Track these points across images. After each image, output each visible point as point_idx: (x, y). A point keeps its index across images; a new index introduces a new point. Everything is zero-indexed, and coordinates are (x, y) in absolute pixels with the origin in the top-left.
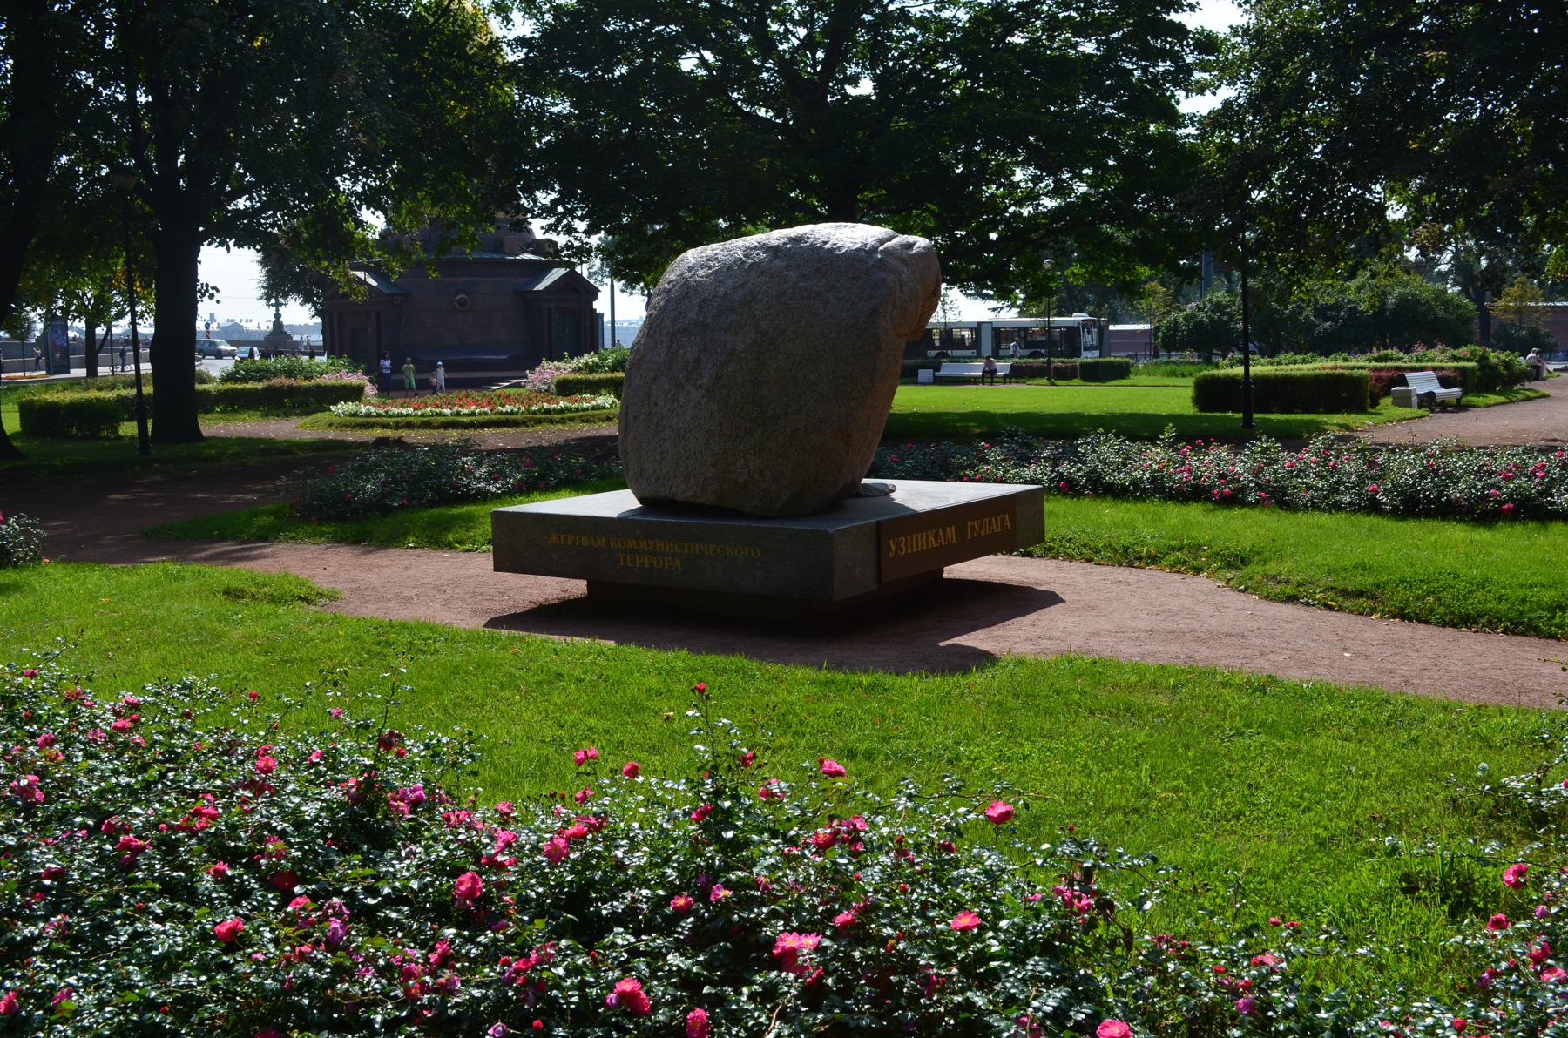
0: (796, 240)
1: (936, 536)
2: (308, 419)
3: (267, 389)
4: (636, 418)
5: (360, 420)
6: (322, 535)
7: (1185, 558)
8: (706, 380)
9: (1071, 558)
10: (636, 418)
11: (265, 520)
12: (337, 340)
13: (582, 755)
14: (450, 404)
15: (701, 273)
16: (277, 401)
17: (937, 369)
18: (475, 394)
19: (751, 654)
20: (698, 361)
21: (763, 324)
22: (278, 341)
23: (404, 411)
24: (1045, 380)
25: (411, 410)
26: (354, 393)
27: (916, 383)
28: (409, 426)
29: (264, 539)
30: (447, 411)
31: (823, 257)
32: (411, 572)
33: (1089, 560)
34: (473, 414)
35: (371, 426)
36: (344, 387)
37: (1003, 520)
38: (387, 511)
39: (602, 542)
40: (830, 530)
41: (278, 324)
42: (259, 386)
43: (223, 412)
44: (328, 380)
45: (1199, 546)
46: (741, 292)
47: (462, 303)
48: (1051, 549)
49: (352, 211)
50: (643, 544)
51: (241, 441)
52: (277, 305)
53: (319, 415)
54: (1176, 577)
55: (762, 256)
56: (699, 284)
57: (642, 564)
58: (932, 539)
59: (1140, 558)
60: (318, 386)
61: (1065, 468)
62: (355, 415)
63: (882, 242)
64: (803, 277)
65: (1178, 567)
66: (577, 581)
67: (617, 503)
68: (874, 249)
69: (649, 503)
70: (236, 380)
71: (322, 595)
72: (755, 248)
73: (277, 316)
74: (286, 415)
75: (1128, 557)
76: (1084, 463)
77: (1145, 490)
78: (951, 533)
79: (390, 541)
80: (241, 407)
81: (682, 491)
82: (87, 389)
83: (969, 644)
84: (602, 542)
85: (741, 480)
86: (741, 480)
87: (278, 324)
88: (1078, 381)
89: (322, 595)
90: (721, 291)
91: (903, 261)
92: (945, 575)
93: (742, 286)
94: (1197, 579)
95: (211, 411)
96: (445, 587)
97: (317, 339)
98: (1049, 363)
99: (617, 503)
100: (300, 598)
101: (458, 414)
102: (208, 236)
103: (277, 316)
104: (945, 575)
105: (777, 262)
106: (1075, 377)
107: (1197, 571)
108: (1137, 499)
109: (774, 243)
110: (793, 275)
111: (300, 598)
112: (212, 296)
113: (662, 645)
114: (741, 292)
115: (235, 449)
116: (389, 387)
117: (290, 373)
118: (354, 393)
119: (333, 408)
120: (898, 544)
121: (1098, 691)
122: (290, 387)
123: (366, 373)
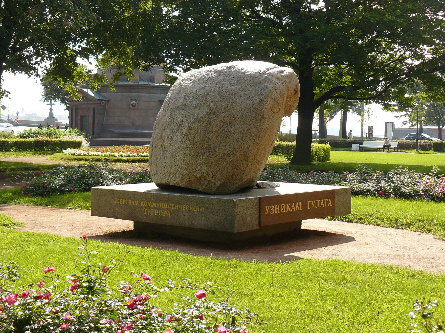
0: (229, 68)
1: (291, 207)
2: (52, 156)
3: (36, 142)
4: (156, 147)
5: (75, 157)
6: (32, 202)
7: (423, 226)
8: (185, 130)
9: (370, 224)
10: (156, 147)
11: (8, 195)
12: (76, 122)
13: (47, 269)
14: (119, 151)
15: (187, 82)
16: (39, 147)
17: (361, 144)
18: (131, 147)
19: (180, 251)
20: (182, 121)
21: (211, 105)
22: (51, 121)
23: (97, 154)
24: (415, 151)
25: (99, 153)
26: (77, 145)
27: (351, 150)
28: (98, 160)
29: (5, 203)
30: (116, 154)
31: (241, 77)
32: (63, 218)
33: (378, 225)
34: (129, 156)
35: (81, 160)
36: (72, 142)
37: (327, 202)
38: (63, 192)
39: (137, 203)
40: (235, 200)
41: (51, 114)
42: (32, 140)
43: (14, 151)
44: (66, 139)
45: (432, 220)
46: (203, 90)
47: (133, 106)
48: (361, 219)
49: (73, 58)
50: (154, 204)
51: (17, 163)
52: (51, 104)
53: (58, 154)
54: (417, 233)
55: (213, 74)
56: (186, 87)
57: (154, 213)
58: (288, 207)
59: (402, 225)
60: (60, 141)
61: (383, 184)
62: (73, 154)
63: (268, 70)
64: (231, 85)
65: (421, 229)
66: (127, 222)
67: (151, 187)
68: (264, 73)
69: (163, 187)
70: (25, 137)
71: (15, 224)
72: (211, 71)
73: (51, 110)
74: (44, 154)
75: (397, 224)
76: (392, 182)
77: (420, 196)
78: (299, 206)
79: (63, 205)
80: (23, 150)
81: (172, 181)
82: (102, 185)
83: (296, 255)
84: (137, 203)
85: (198, 176)
86: (198, 176)
87: (51, 114)
88: (432, 152)
89: (15, 224)
90: (194, 91)
91: (278, 78)
92: (303, 227)
93: (204, 88)
94: (428, 235)
95: (9, 150)
96: (73, 222)
97: (66, 121)
98: (417, 142)
99: (151, 187)
100: (4, 225)
101: (121, 156)
102: (6, 68)
103: (51, 110)
104: (303, 227)
105: (220, 78)
106: (430, 149)
107: (428, 231)
108: (415, 199)
109: (220, 69)
110: (226, 83)
111: (4, 225)
112: (7, 96)
113: (146, 246)
114: (203, 90)
115: (13, 167)
116: (93, 144)
117: (49, 135)
118: (77, 145)
119: (64, 151)
120: (270, 208)
121: (373, 286)
122: (47, 141)
123: (86, 136)
